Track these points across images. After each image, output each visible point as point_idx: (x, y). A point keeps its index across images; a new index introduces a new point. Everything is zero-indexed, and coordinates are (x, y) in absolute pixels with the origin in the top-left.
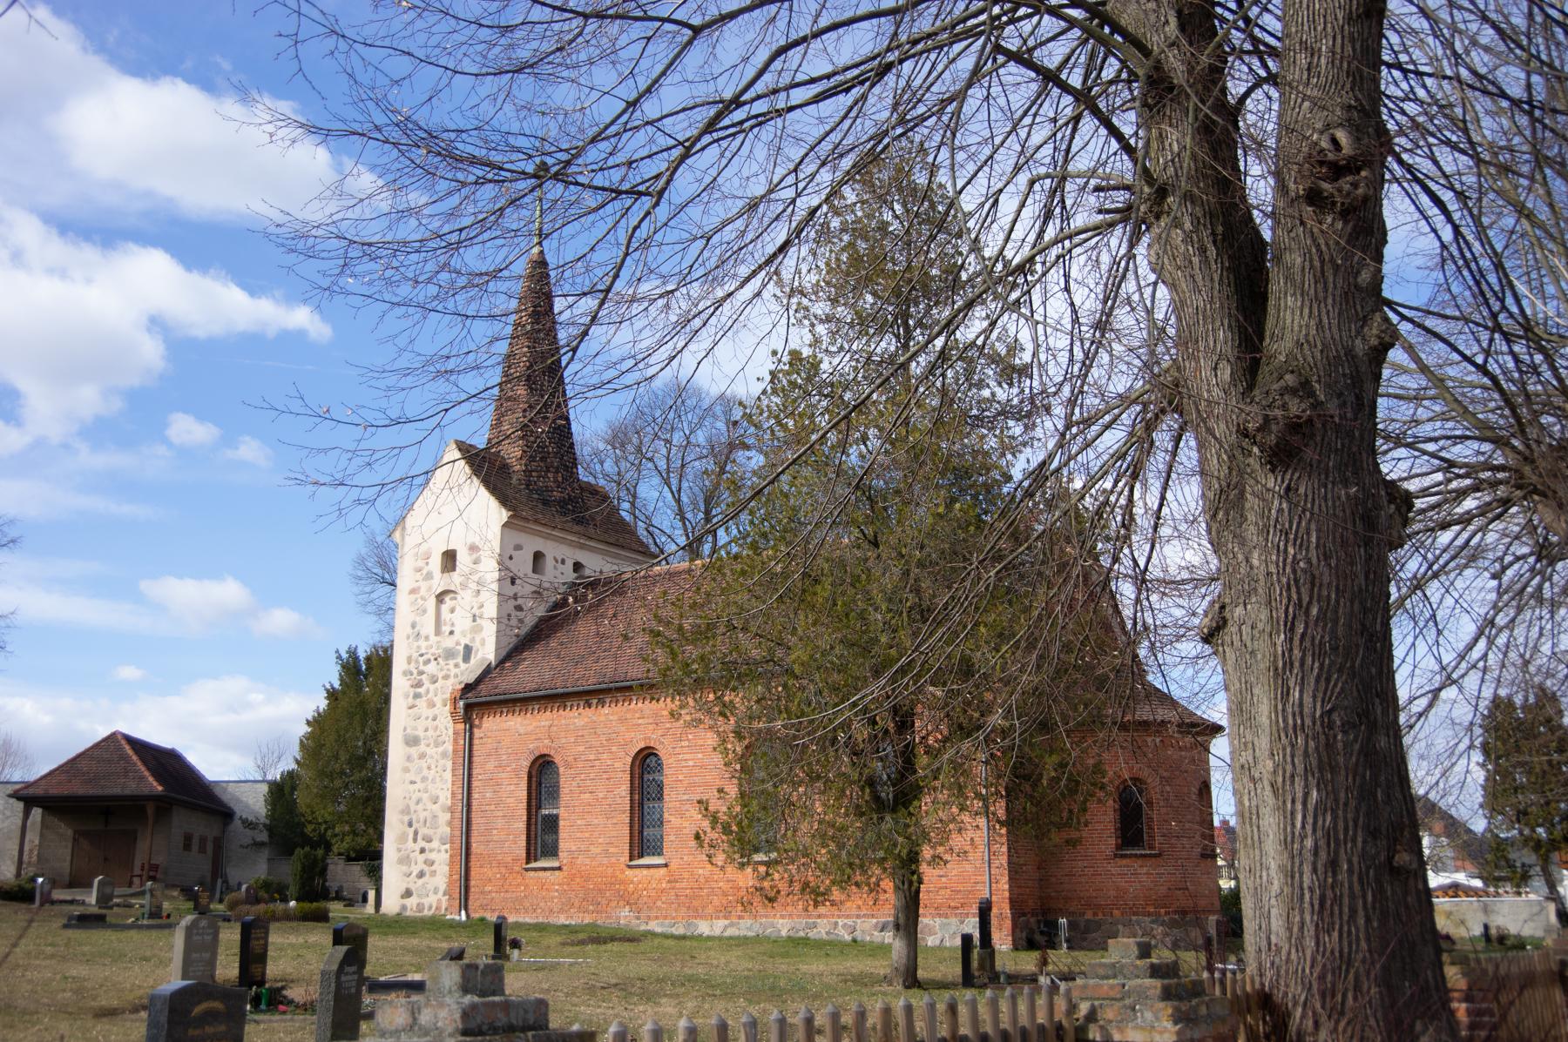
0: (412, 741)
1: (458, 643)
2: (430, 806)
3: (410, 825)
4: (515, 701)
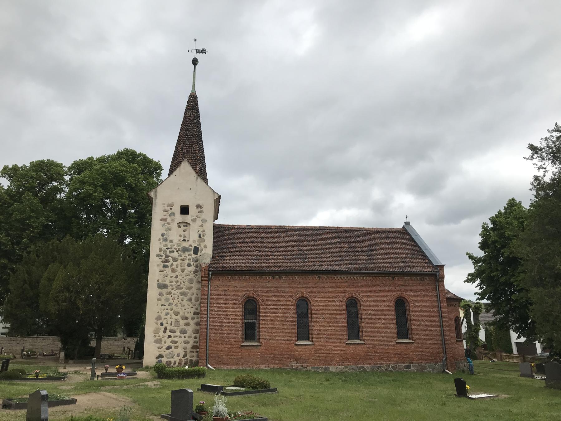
0: (162, 286)
2: (174, 316)
3: (162, 324)
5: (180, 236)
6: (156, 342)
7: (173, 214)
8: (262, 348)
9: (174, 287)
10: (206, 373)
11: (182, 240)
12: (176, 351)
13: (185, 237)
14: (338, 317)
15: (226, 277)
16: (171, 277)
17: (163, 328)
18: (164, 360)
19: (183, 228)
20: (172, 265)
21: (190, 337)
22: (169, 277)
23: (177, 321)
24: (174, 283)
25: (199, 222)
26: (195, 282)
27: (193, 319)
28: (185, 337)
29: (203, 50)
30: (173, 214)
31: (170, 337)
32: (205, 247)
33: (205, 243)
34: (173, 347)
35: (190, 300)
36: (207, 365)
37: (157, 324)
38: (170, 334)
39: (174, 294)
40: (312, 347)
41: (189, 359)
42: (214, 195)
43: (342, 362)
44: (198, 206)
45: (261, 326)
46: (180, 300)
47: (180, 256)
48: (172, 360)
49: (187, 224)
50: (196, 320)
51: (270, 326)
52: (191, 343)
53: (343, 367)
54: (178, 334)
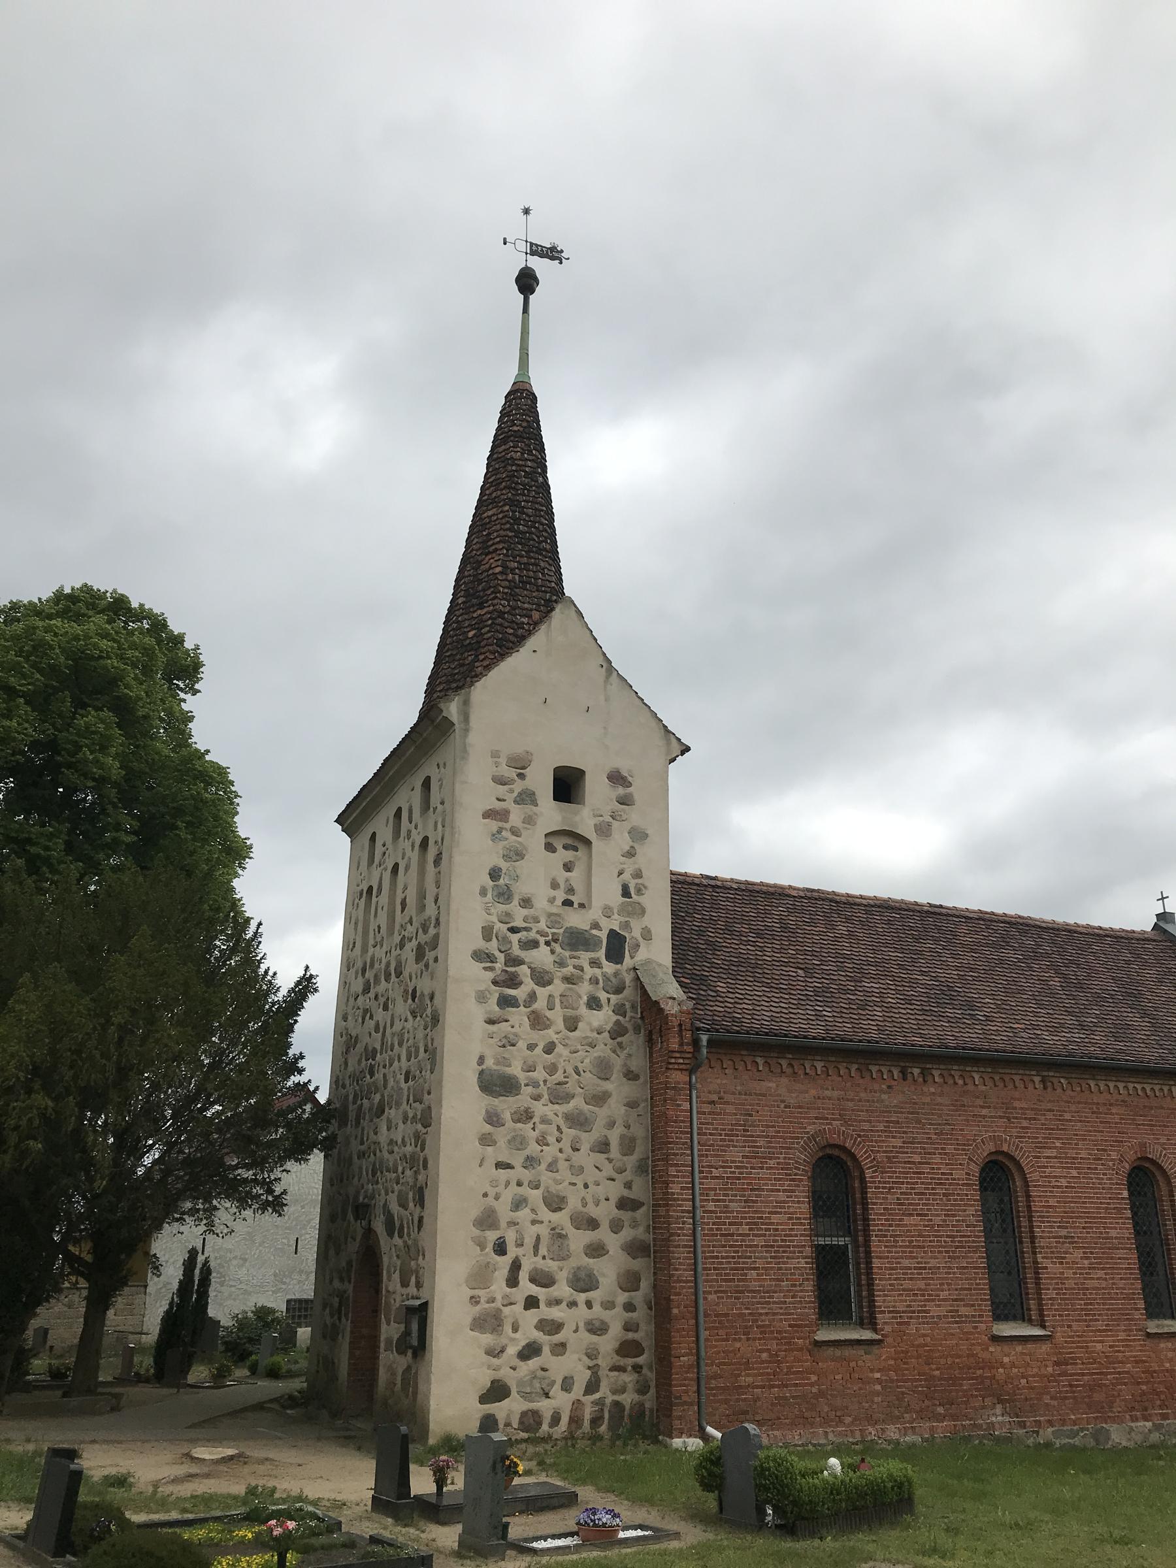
0: (496, 1084)
1: (596, 926)
2: (545, 1214)
3: (500, 1249)
4: (1070, 1066)
5: (555, 885)
6: (479, 1324)
7: (527, 798)
8: (885, 1352)
9: (543, 1090)
10: (919, 1492)
11: (559, 902)
12: (560, 1366)
13: (571, 890)
14: (1113, 1233)
15: (749, 1060)
16: (531, 1047)
17: (504, 1262)
18: (510, 1409)
19: (563, 855)
20: (532, 997)
21: (608, 1305)
22: (522, 1045)
23: (558, 1236)
24: (539, 1074)
25: (621, 838)
26: (617, 1075)
27: (616, 1227)
28: (589, 1305)
29: (553, 249)
30: (527, 798)
31: (531, 1303)
32: (647, 935)
33: (646, 921)
34: (546, 1350)
35: (603, 1147)
36: (702, 1430)
37: (482, 1246)
38: (534, 1290)
39: (545, 1121)
40: (1045, 1348)
41: (608, 1401)
42: (668, 743)
43: (1140, 1407)
44: (617, 778)
45: (876, 1263)
46: (566, 1144)
47: (561, 964)
48: (545, 1407)
49: (575, 840)
50: (627, 1234)
51: (906, 1263)
52: (616, 1330)
53: (1149, 1424)
54: (562, 1289)
